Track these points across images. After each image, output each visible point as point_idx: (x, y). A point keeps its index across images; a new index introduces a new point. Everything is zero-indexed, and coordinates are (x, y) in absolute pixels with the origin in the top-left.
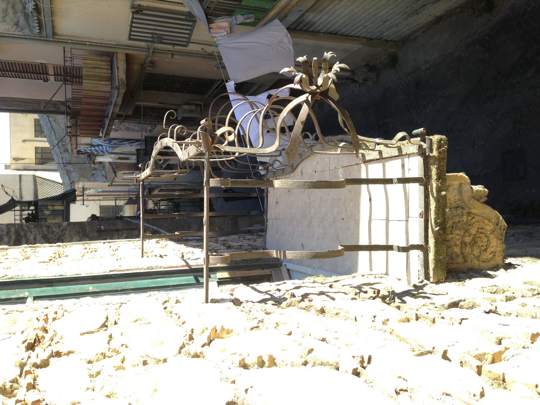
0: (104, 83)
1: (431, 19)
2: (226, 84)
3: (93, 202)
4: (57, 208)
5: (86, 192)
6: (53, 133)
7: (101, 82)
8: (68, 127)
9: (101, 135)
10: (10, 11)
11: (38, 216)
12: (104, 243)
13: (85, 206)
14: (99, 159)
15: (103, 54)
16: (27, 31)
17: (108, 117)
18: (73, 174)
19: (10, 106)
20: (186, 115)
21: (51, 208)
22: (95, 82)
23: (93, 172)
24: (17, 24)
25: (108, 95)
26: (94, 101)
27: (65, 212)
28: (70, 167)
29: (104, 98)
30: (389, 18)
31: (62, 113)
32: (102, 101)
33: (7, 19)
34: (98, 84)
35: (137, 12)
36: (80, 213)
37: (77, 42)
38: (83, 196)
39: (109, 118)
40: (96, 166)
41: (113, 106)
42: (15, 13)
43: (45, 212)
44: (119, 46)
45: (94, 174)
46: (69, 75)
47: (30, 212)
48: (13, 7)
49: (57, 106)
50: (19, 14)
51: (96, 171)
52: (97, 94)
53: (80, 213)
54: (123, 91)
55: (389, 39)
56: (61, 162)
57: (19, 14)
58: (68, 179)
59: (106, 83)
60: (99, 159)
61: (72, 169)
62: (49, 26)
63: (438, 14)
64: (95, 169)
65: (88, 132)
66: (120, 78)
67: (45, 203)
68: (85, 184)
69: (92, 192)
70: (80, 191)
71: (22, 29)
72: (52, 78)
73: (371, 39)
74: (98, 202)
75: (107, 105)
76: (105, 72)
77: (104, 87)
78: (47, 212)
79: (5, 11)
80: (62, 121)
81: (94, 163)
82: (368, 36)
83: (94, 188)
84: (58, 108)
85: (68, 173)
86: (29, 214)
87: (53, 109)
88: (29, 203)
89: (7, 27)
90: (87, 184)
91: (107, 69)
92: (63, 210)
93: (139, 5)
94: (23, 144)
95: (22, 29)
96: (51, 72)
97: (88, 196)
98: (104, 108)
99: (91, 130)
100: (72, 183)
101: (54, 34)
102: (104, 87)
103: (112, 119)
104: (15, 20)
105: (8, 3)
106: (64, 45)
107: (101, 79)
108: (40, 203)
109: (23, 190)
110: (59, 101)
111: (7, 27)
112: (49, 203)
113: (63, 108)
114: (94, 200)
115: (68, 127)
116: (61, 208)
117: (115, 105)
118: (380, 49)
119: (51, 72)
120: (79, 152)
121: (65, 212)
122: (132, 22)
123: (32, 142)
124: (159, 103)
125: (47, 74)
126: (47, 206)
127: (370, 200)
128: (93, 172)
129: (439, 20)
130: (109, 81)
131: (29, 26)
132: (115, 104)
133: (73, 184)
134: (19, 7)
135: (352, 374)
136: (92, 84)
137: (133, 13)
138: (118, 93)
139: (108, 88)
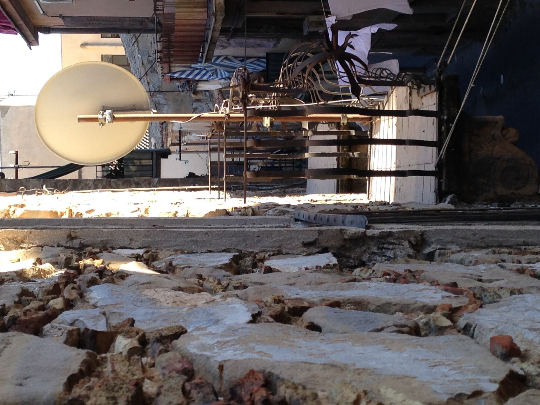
0: (198, 10)
2: (326, 19)
3: (196, 155)
4: (144, 162)
5: (184, 138)
7: (195, 10)
8: (158, 52)
11: (123, 173)
12: (84, 45)
14: (202, 86)
17: (207, 41)
19: (86, 26)
20: (312, 30)
21: (137, 162)
22: (190, 10)
23: (195, 105)
25: (205, 22)
26: (188, 28)
27: (155, 168)
29: (200, 25)
31: (151, 31)
34: (192, 12)
38: (179, 144)
39: (209, 42)
40: (199, 96)
41: (211, 32)
43: (131, 167)
49: (144, 23)
51: (199, 104)
53: (170, 168)
59: (202, 10)
60: (202, 86)
61: (163, 101)
64: (198, 100)
65: (187, 58)
66: (217, 2)
69: (193, 137)
70: (176, 137)
74: (204, 155)
78: (133, 168)
80: (150, 41)
83: (197, 132)
92: (152, 166)
94: (81, 50)
97: (187, 144)
98: (202, 34)
99: (189, 56)
103: (213, 44)
110: (148, 18)
112: (136, 156)
113: (151, 26)
114: (197, 152)
115: (158, 52)
116: (149, 162)
117: (214, 30)
120: (172, 79)
121: (155, 168)
123: (96, 47)
124: (277, 14)
128: (195, 105)
130: (204, 7)
132: (213, 29)
133: (164, 126)
135: (190, 173)
136: (186, 12)
138: (216, 20)
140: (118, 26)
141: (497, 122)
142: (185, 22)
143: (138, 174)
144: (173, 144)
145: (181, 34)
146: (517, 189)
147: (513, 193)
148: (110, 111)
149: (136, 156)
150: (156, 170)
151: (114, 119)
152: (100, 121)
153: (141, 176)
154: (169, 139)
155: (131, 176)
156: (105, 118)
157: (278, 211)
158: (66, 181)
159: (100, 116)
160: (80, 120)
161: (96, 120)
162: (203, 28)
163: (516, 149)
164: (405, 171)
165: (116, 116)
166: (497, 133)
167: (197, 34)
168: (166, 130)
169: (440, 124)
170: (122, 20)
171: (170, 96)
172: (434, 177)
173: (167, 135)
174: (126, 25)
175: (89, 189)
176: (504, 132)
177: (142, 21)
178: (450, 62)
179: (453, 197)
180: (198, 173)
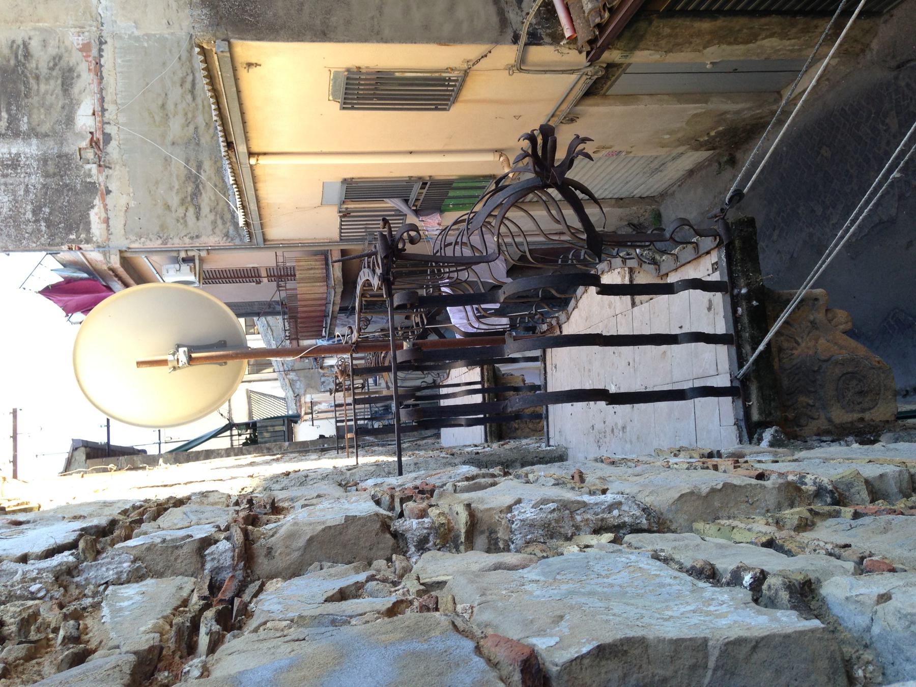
1: (681, 173)
3: (326, 421)
4: (277, 428)
5: (316, 408)
6: (269, 331)
9: (324, 333)
10: (219, 222)
13: (315, 428)
15: (316, 253)
16: (237, 241)
18: (298, 384)
23: (323, 379)
24: (227, 235)
25: (325, 296)
28: (292, 375)
29: (321, 299)
30: (629, 179)
31: (278, 313)
32: (319, 302)
33: (217, 231)
35: (344, 216)
36: (305, 432)
37: (288, 245)
38: (312, 413)
40: (326, 371)
42: (224, 223)
44: (332, 242)
45: (324, 382)
46: (282, 275)
47: (248, 436)
48: (222, 218)
50: (229, 224)
52: (313, 296)
53: (305, 432)
54: (340, 290)
55: (645, 196)
56: (282, 369)
57: (229, 224)
58: (291, 392)
62: (259, 232)
63: (688, 168)
67: (264, 424)
68: (314, 396)
69: (323, 406)
71: (232, 240)
72: (265, 280)
73: (622, 199)
75: (326, 305)
76: (320, 273)
77: (319, 289)
78: (267, 435)
79: (214, 223)
81: (321, 368)
82: (616, 196)
83: (325, 402)
84: (274, 308)
85: (292, 384)
86: (246, 439)
87: (267, 310)
88: (247, 426)
89: (217, 239)
90: (317, 397)
91: (315, 280)
93: (347, 208)
95: (232, 240)
96: (264, 274)
98: (324, 308)
100: (297, 397)
101: (265, 240)
102: (319, 289)
103: (334, 318)
104: (225, 231)
105: (216, 214)
106: (275, 250)
107: (315, 280)
108: (258, 425)
109: (233, 412)
111: (217, 239)
112: (269, 423)
113: (279, 308)
114: (327, 418)
118: (635, 208)
119: (264, 274)
122: (341, 225)
125: (259, 276)
126: (251, 166)
127: (14, 437)
128: (323, 379)
129: (691, 173)
131: (240, 235)
134: (228, 216)
137: (341, 217)
139: (324, 289)
140: (249, 311)
141: (816, 299)
142: (308, 296)
143: (272, 439)
144: (306, 414)
145: (305, 309)
146: (863, 411)
147: (862, 420)
148: (186, 349)
149: (269, 423)
150: (290, 434)
151: (190, 360)
152: (170, 365)
153: (275, 441)
154: (303, 410)
155: (265, 442)
156: (178, 360)
157: (552, 506)
158: (198, 453)
159: (170, 358)
160: (140, 364)
161: (164, 362)
162: (324, 302)
163: (853, 343)
164: (683, 390)
165: (193, 355)
166: (820, 316)
167: (319, 308)
168: (300, 401)
169: (735, 302)
170: (251, 304)
171: (302, 373)
172: (730, 398)
173: (300, 406)
174: (256, 309)
175: (222, 457)
176: (830, 315)
177: (269, 304)
178: (752, 188)
179: (776, 431)
180: (327, 435)
